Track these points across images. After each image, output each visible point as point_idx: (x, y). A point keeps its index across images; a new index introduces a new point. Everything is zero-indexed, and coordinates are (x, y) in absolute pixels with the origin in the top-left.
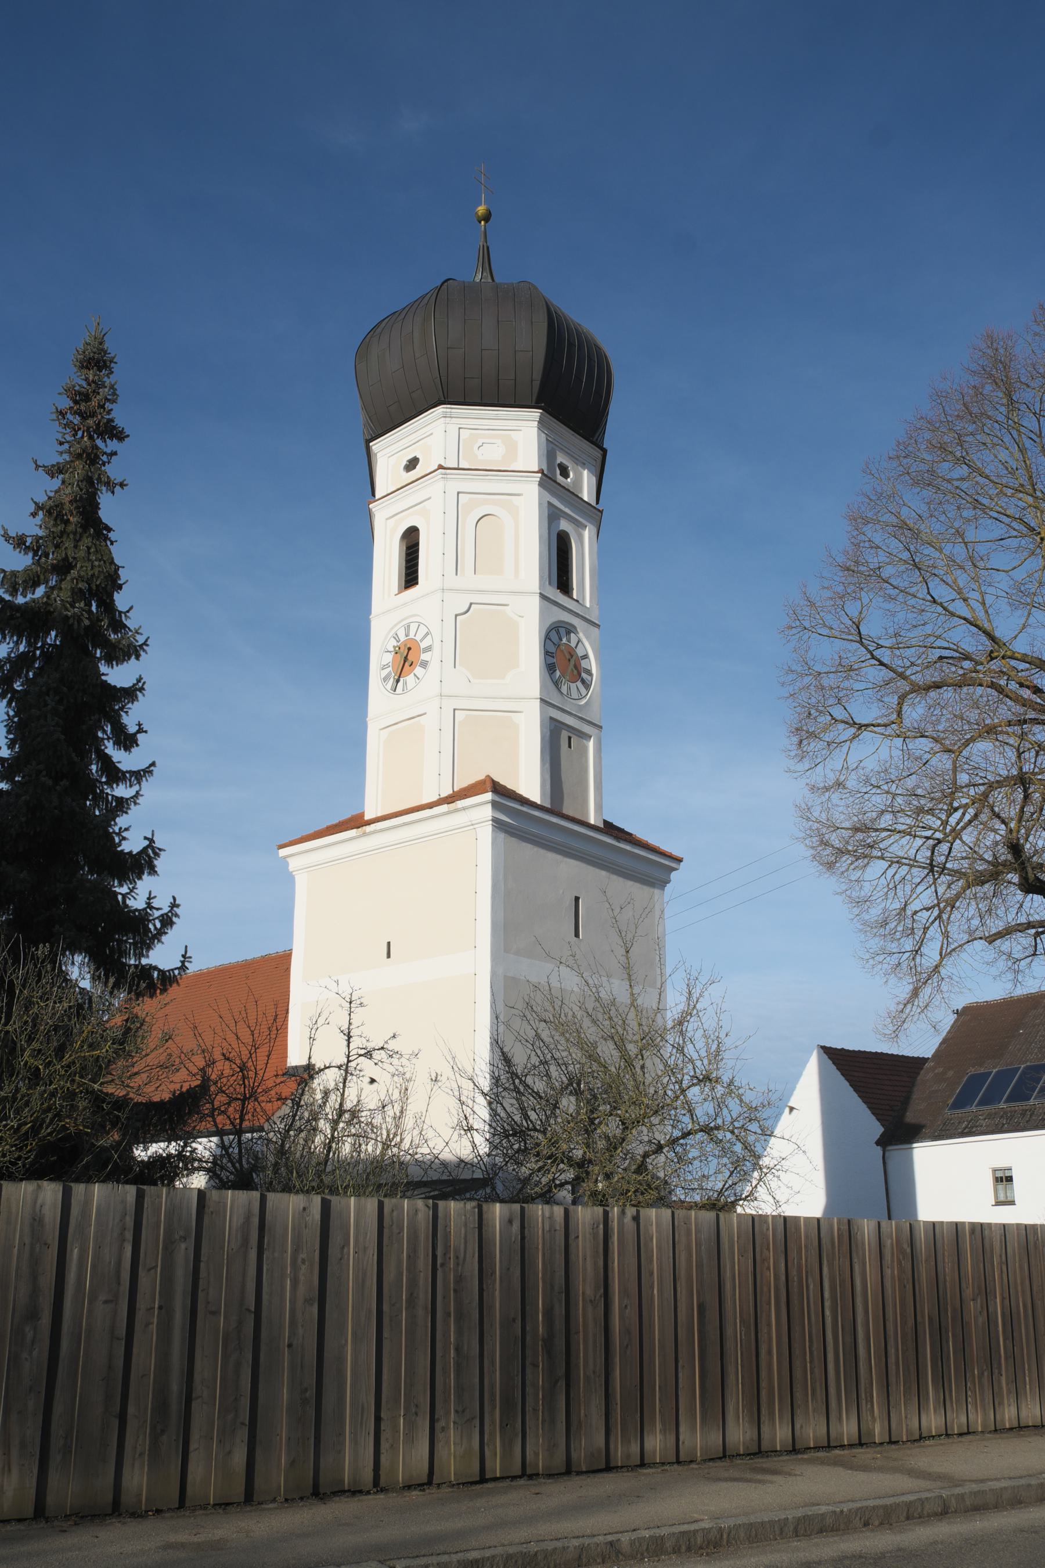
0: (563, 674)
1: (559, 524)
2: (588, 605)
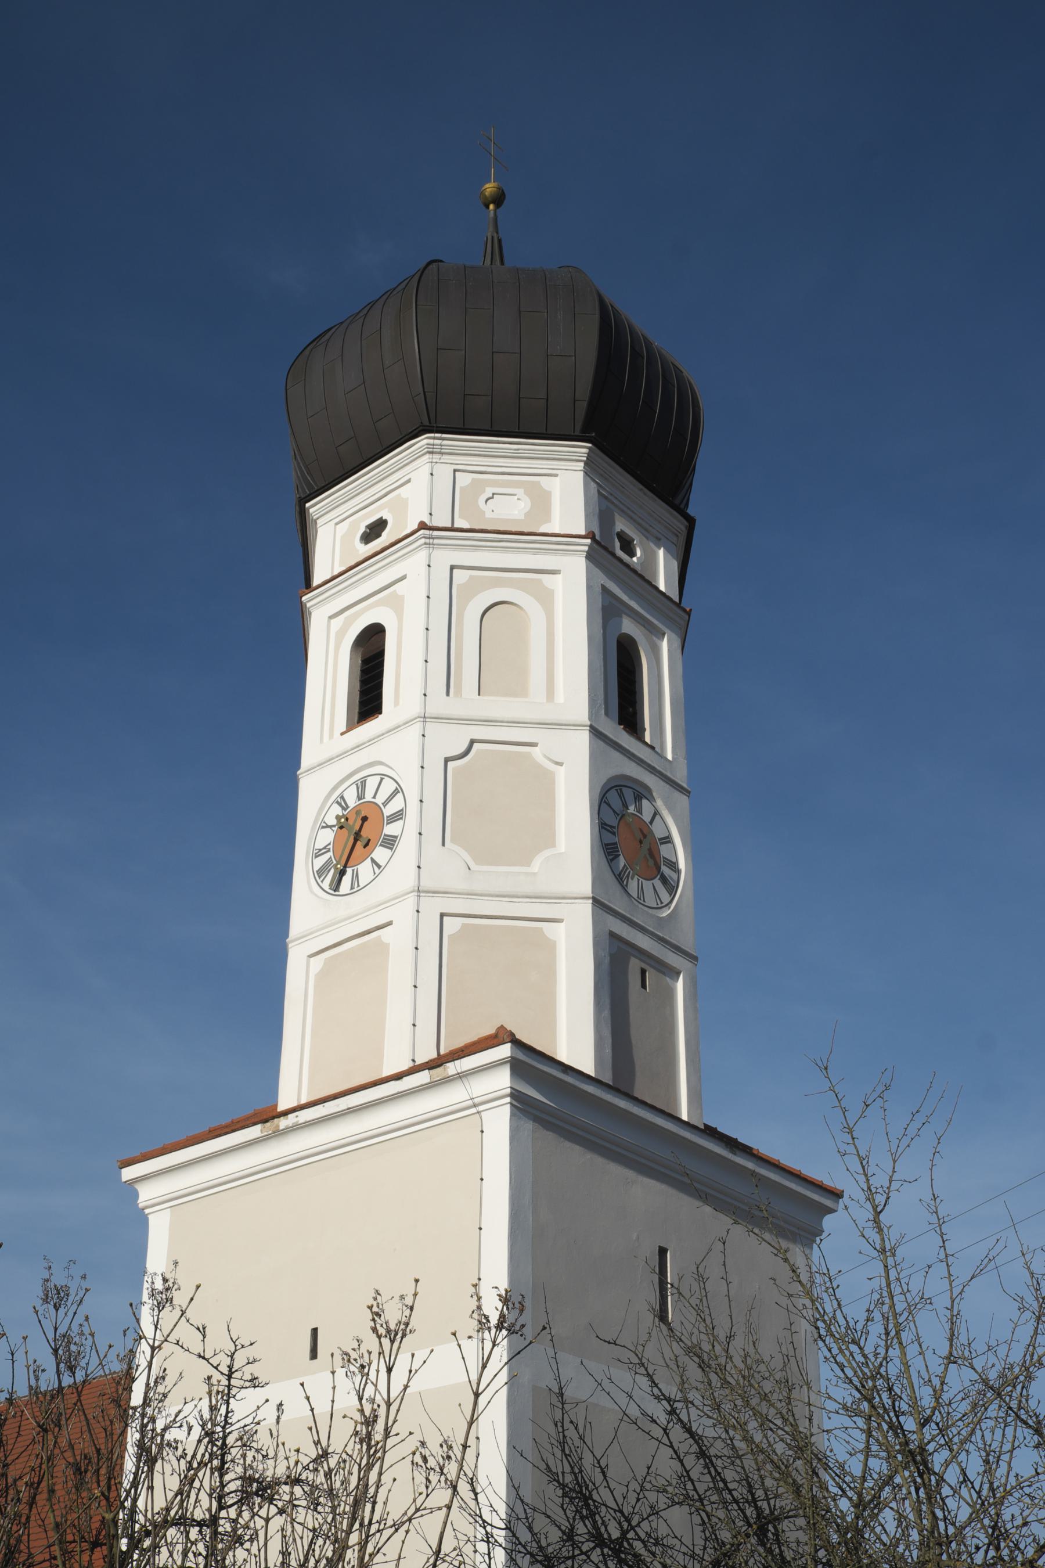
0: (630, 863)
1: (621, 622)
2: (670, 757)
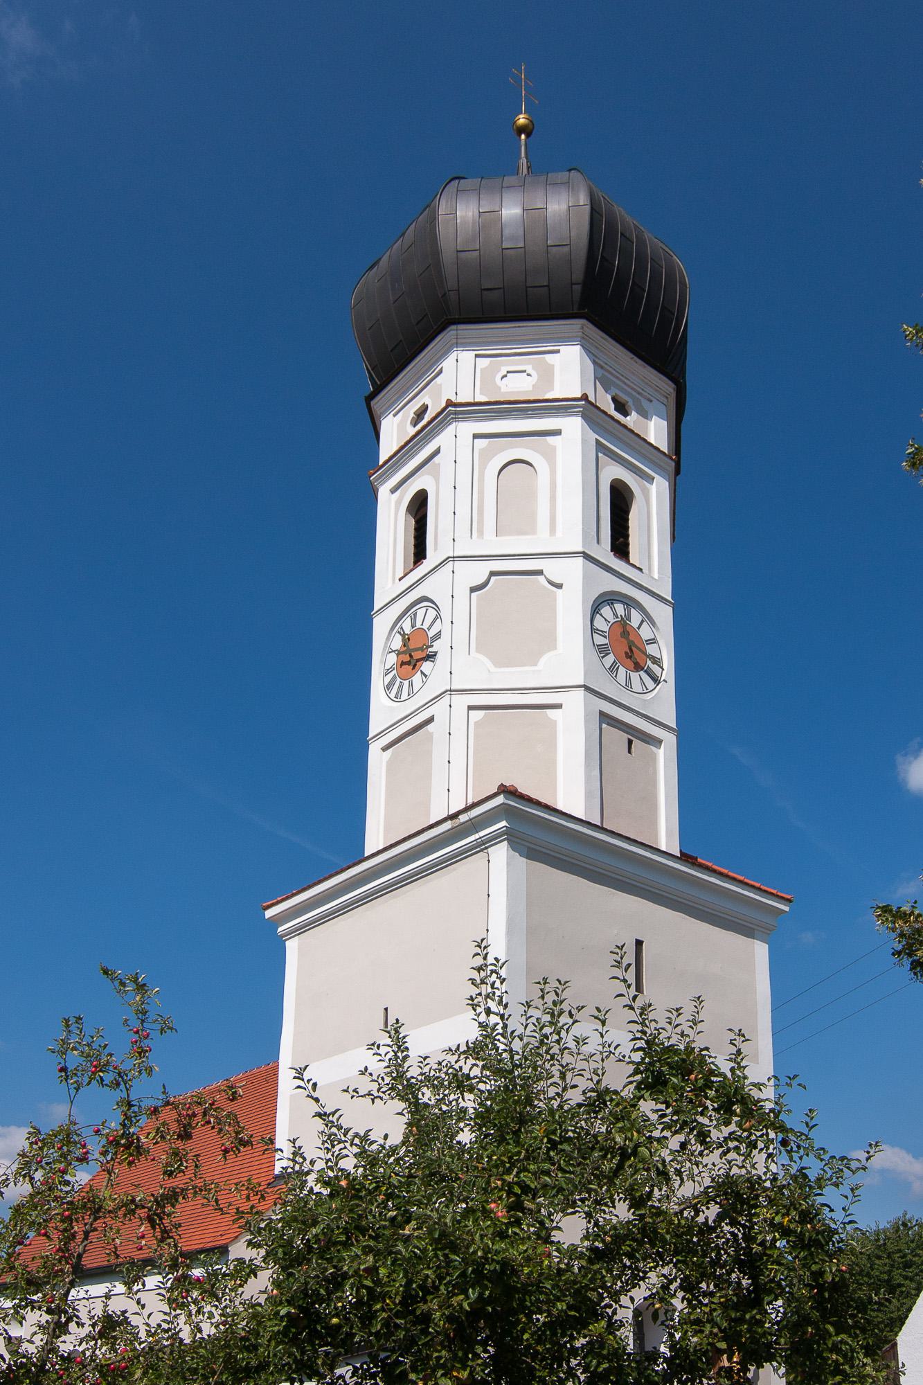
2: (656, 576)
